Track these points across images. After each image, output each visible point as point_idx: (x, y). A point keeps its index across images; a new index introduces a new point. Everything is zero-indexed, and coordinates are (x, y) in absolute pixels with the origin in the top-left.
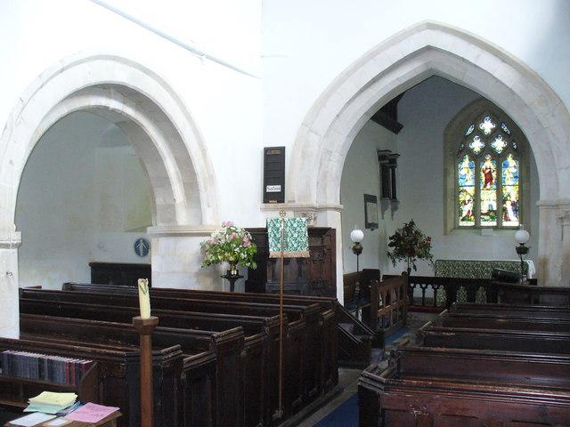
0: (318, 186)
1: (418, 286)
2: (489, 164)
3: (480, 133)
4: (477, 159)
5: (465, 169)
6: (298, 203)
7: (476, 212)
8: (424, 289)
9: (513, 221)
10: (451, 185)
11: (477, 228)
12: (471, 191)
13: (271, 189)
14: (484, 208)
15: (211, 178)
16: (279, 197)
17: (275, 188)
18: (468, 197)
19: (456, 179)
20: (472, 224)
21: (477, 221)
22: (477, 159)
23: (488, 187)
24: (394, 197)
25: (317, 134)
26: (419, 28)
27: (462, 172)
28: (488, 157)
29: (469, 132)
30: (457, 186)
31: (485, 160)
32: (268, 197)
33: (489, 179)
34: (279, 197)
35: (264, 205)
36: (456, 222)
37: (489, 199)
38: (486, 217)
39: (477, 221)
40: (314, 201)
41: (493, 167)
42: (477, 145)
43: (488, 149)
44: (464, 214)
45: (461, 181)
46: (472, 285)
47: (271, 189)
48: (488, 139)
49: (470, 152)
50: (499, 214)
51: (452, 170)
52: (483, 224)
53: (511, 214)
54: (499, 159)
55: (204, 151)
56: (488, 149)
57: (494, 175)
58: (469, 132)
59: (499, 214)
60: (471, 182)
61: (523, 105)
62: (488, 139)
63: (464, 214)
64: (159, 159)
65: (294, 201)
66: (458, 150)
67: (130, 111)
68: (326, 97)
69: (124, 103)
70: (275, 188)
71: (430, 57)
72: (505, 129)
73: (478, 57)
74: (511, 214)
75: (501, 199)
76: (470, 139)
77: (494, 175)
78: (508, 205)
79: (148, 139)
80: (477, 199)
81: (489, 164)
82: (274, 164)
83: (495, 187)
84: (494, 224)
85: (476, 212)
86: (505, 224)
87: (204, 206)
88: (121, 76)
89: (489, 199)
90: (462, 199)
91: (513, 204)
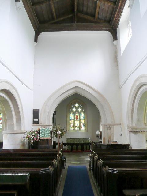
0: (46, 119)
1: (85, 145)
2: (77, 114)
3: (75, 107)
4: (74, 113)
5: (71, 115)
6: (42, 124)
7: (74, 126)
8: (65, 146)
9: (83, 128)
10: (68, 120)
11: (74, 130)
12: (73, 121)
13: (35, 120)
14: (76, 125)
15: (24, 117)
16: (37, 123)
17: (37, 120)
18: (72, 122)
19: (69, 118)
20: (73, 129)
21: (74, 128)
22: (74, 113)
23: (77, 120)
24: (55, 122)
25: (48, 106)
26: (74, 82)
27: (71, 116)
28: (77, 113)
29: (72, 106)
30: (69, 120)
31: (76, 113)
32: (34, 123)
33: (77, 118)
34: (37, 123)
35: (33, 125)
36: (69, 128)
37: (77, 123)
38: (77, 127)
39: (74, 128)
40: (47, 124)
41: (78, 115)
42: (74, 110)
43: (77, 111)
44: (71, 126)
45: (70, 119)
46: (77, 145)
47: (35, 120)
48: (77, 108)
49: (73, 111)
50: (80, 126)
51: (68, 116)
52: (76, 129)
53: (83, 126)
54: (80, 113)
55: (22, 110)
56: (77, 111)
57: (78, 117)
58: (72, 106)
59: (80, 126)
60: (73, 119)
61: (98, 101)
62: (77, 108)
63: (71, 126)
64: (11, 111)
65: (41, 124)
66: (70, 111)
67: (6, 97)
68: (51, 97)
69: (5, 95)
70: (37, 120)
71: (76, 89)
72: (81, 106)
73: (88, 90)
74: (83, 126)
75: (80, 123)
76: (73, 108)
77: (78, 117)
78: (82, 124)
79: (9, 106)
80: (74, 123)
81: (77, 114)
82: (36, 114)
83: (79, 120)
84: (79, 129)
85: (74, 126)
86: (81, 129)
87: (22, 125)
88: (8, 87)
89: (77, 123)
90: (70, 123)
91: (83, 124)
